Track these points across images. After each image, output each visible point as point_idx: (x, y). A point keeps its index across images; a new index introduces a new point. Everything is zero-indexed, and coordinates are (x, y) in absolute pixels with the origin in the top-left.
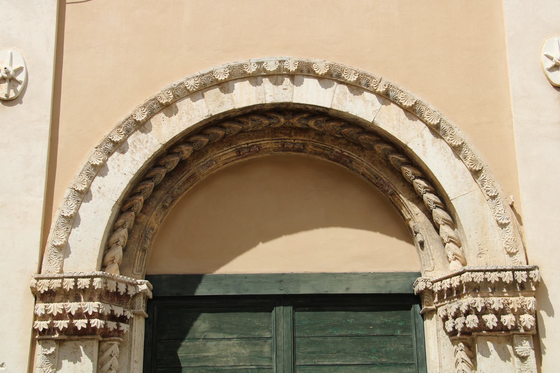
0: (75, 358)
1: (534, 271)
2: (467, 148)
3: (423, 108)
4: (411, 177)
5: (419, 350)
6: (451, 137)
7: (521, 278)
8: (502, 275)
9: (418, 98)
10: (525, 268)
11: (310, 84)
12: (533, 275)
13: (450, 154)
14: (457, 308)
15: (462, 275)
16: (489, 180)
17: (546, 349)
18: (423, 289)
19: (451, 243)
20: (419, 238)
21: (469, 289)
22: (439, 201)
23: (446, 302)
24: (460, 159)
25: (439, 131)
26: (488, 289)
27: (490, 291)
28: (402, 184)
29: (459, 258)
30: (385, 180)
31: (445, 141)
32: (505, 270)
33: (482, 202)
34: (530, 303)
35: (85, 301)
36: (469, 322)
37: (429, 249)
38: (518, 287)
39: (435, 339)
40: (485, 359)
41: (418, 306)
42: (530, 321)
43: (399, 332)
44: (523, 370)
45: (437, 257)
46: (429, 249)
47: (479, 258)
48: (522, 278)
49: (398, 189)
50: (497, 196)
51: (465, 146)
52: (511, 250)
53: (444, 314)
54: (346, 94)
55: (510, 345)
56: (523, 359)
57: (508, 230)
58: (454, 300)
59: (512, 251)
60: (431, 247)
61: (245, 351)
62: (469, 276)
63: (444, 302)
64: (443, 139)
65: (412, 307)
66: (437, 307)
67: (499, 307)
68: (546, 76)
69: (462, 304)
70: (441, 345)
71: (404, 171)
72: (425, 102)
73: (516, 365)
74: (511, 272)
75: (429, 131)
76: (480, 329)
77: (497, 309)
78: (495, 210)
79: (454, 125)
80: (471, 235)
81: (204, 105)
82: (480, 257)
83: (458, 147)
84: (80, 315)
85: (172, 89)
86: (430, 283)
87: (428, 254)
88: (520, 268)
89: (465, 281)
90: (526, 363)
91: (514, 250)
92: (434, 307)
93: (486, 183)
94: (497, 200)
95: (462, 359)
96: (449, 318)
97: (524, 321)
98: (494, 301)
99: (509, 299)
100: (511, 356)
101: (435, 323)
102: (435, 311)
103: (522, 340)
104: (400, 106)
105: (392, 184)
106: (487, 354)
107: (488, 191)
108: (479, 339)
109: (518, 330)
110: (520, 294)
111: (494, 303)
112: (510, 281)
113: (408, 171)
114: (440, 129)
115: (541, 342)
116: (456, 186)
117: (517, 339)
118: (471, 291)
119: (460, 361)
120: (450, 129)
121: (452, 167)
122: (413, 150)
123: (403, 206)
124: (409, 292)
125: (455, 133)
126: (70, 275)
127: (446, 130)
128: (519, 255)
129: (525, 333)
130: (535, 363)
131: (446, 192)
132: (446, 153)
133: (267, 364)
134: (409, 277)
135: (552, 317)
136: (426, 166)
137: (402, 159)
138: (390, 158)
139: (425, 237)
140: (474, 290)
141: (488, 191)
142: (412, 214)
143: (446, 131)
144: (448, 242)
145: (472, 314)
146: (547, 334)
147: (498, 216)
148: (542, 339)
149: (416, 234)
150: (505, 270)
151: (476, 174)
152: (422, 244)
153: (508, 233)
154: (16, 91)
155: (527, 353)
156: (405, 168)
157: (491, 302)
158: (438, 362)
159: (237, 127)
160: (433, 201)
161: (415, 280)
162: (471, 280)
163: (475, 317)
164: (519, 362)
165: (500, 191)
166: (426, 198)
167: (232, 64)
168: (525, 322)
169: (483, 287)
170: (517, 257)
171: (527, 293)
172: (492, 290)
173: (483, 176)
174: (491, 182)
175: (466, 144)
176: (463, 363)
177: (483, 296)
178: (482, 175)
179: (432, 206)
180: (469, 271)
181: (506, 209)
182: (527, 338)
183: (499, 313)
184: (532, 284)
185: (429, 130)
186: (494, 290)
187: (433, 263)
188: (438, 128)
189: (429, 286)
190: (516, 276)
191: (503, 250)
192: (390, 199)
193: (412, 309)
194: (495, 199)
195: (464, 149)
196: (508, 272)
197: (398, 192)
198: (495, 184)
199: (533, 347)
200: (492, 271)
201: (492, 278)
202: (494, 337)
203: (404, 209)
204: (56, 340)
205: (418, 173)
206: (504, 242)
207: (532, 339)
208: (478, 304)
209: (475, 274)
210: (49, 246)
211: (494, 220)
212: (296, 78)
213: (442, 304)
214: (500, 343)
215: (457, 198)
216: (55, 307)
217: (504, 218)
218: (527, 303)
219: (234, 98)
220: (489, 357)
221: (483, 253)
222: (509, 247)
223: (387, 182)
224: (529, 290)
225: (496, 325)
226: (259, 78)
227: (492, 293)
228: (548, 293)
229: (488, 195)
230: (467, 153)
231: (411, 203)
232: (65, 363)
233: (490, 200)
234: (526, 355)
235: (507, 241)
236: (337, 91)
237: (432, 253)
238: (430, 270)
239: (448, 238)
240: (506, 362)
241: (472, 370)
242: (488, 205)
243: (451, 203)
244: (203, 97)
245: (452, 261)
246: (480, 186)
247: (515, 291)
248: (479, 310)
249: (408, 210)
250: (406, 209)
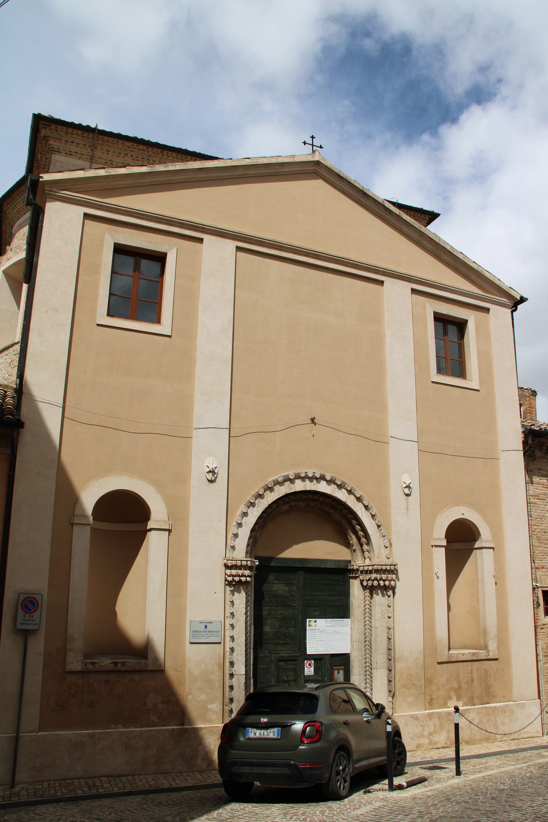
0: (239, 592)
3: (363, 498)
9: (362, 494)
11: (323, 483)
20: (354, 548)
24: (374, 520)
32: (388, 565)
35: (244, 570)
41: (348, 573)
43: (341, 583)
54: (336, 489)
56: (389, 596)
61: (286, 589)
66: (359, 576)
68: (403, 490)
72: (364, 496)
79: (373, 506)
81: (284, 489)
84: (243, 575)
85: (273, 481)
92: (358, 575)
102: (359, 577)
104: (355, 496)
106: (378, 595)
113: (354, 522)
119: (367, 612)
126: (239, 559)
133: (294, 594)
150: (388, 565)
151: (379, 526)
152: (354, 550)
154: (214, 477)
159: (293, 497)
163: (377, 582)
167: (296, 472)
179: (361, 537)
183: (384, 581)
200: (384, 565)
204: (234, 584)
205: (357, 523)
210: (228, 546)
212: (318, 480)
214: (382, 590)
216: (234, 572)
219: (295, 486)
226: (305, 479)
232: (236, 593)
236: (333, 487)
244: (284, 485)
248: (379, 579)
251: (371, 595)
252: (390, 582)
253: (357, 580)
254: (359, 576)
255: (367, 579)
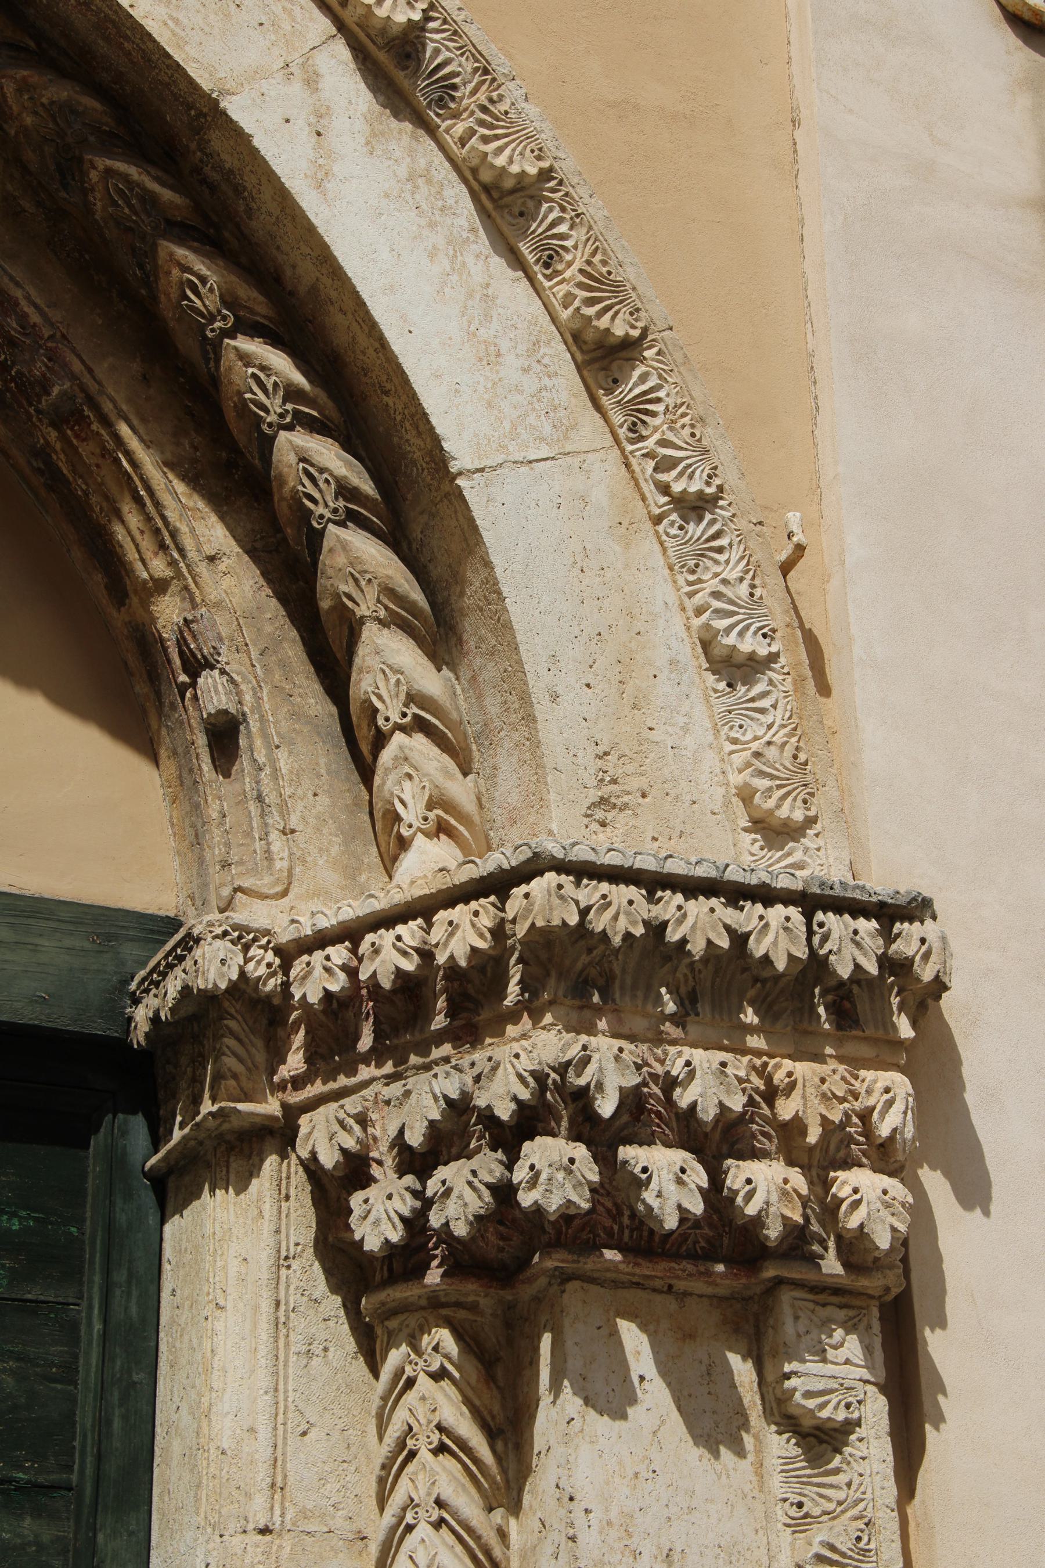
1: (917, 924)
2: (563, 209)
4: (212, 319)
5: (116, 1394)
6: (482, 123)
7: (850, 951)
8: (749, 919)
10: (874, 899)
12: (915, 944)
13: (462, 221)
14: (454, 1095)
15: (518, 891)
16: (677, 407)
17: (945, 1394)
18: (223, 986)
19: (419, 742)
21: (552, 982)
22: (367, 487)
23: (365, 1072)
24: (517, 261)
25: (416, 73)
26: (660, 995)
27: (671, 1007)
28: (136, 367)
29: (461, 828)
30: (35, 318)
31: (442, 147)
32: (766, 896)
33: (625, 523)
34: (890, 1103)
36: (537, 1176)
37: (268, 770)
38: (821, 1010)
39: (256, 1308)
40: (601, 1424)
41: (138, 1126)
42: (888, 1206)
44: (816, 1511)
45: (312, 820)
46: (268, 770)
47: (595, 826)
48: (857, 953)
49: (110, 390)
50: (714, 500)
51: (553, 191)
52: (778, 806)
53: (350, 1143)
55: (744, 1359)
57: (764, 695)
58: (427, 1054)
59: (783, 812)
60: (284, 760)
62: (562, 898)
63: (354, 1072)
64: (431, 131)
65: (97, 1131)
66: (292, 1114)
67: (721, 1104)
69: (494, 1069)
70: (293, 1349)
71: (175, 272)
73: (776, 1484)
74: (794, 913)
75: (352, 66)
76: (584, 1236)
77: (708, 1113)
78: (700, 581)
80: (560, 692)
82: (603, 824)
83: (513, 191)
86: (270, 956)
87: (260, 798)
88: (849, 894)
89: (540, 923)
90: (837, 1471)
91: (792, 808)
92: (271, 1107)
93: (657, 421)
94: (713, 522)
95: (440, 1428)
96: (375, 1171)
97: (857, 1204)
98: (695, 1062)
99: (778, 1066)
100: (745, 1425)
101: (268, 1208)
103: (825, 1325)
105: (74, 350)
107: (665, 465)
108: (573, 1295)
109: (813, 1260)
110: (829, 1050)
111: (691, 1075)
112: (791, 958)
114: (419, 62)
115: (919, 1347)
116: (489, 404)
117: (797, 1318)
118: (560, 993)
119: (423, 1443)
120: (477, 79)
121: (470, 295)
122: (256, 142)
123: (128, 498)
124: (98, 1028)
125: (503, 107)
127: (457, 80)
128: (820, 842)
129: (846, 1282)
130: (890, 1472)
131: (434, 420)
132: (443, 209)
134: (109, 937)
135: (978, 1211)
136: (326, 259)
137: (167, 195)
138: (94, 176)
139: (248, 698)
140: (580, 989)
141: (665, 465)
142: (181, 551)
143: (454, 87)
144: (402, 728)
145: (554, 1135)
146: (953, 1305)
147: (716, 611)
148: (927, 1332)
149: (194, 675)
153: (762, 711)
155: (848, 1406)
156: (181, 253)
157: (677, 1069)
158: (264, 1452)
160: (337, 480)
161: (144, 964)
162: (573, 920)
164: (790, 1460)
165: (729, 476)
166: (292, 458)
168: (862, 1210)
169: (629, 981)
170: (806, 850)
171: (866, 1051)
172: (680, 1002)
173: (644, 378)
174: (686, 420)
175: (561, 183)
176: (445, 1459)
177: (625, 1030)
178: (636, 374)
180: (561, 867)
181: (757, 582)
182: (851, 1313)
184: (895, 1001)
185: (356, 57)
186: (689, 1003)
187: (286, 854)
188: (408, 56)
189: (262, 970)
190: (825, 938)
191: (727, 804)
192: (43, 453)
193: (97, 1142)
194: (700, 519)
195: (551, 210)
196: (777, 913)
197: (108, 407)
198: (709, 435)
199: (882, 1375)
201: (694, 927)
202: (658, 1298)
203: (134, 520)
205: (260, 306)
206: (738, 759)
207: (876, 1327)
208: (600, 1069)
209: (596, 888)
211: (684, 634)
213: (332, 1086)
214: (689, 1336)
215: (493, 468)
217: (747, 628)
218: (877, 1099)
220: (624, 1417)
221: (618, 802)
222: (770, 789)
223: (46, 332)
224: (880, 1034)
225: (697, 1207)
227: (677, 1020)
228: (961, 1077)
229: (664, 489)
230: (562, 237)
231: (180, 487)
233: (674, 516)
234: (841, 1415)
235: (757, 755)
237: (288, 791)
238: (266, 891)
239: (406, 705)
240: (716, 1455)
241: (490, 1509)
242: (657, 547)
243: (459, 493)
245: (420, 840)
246: (622, 432)
247: (806, 1033)
248: (606, 1106)
249: (160, 524)
250: (149, 519)
251: (491, 1434)
252: (821, 1183)
253: (262, 1185)
254: (292, 1114)
255: (415, 1138)
